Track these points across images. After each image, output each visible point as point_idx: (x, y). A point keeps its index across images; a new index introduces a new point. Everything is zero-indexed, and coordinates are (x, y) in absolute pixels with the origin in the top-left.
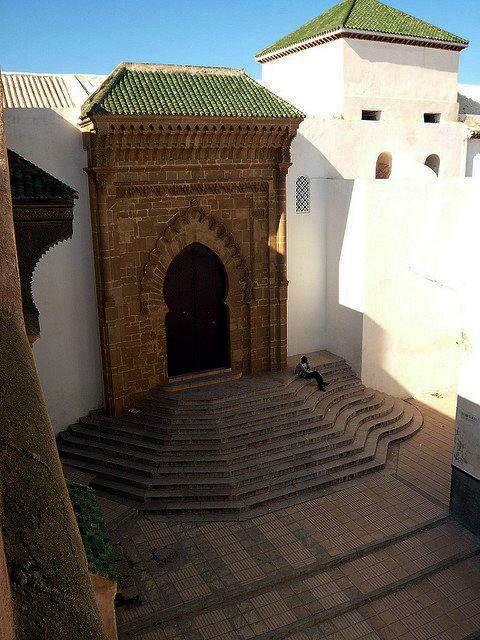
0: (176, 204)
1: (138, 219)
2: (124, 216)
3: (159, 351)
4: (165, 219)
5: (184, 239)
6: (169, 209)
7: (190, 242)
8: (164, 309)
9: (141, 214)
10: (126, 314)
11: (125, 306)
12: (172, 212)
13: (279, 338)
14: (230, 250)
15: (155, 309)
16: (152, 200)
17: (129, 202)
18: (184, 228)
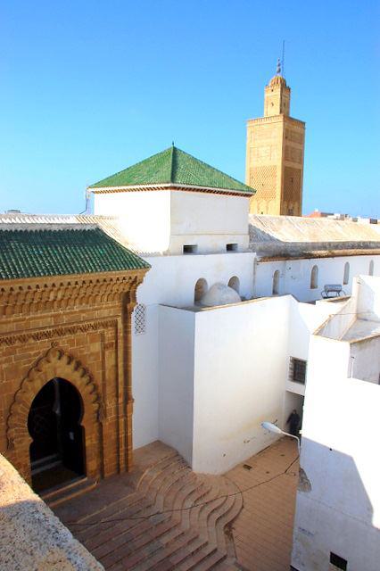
5: (46, 376)
6: (32, 353)
8: (28, 440)
12: (36, 355)
18: (45, 366)
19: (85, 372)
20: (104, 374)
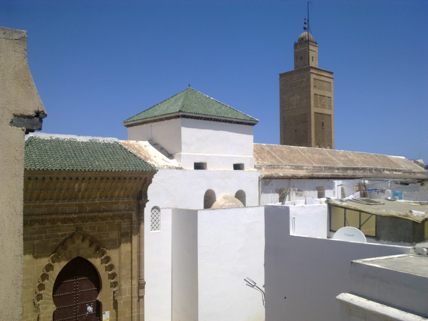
0: (67, 229)
1: (36, 242)
6: (60, 234)
7: (74, 256)
12: (63, 236)
16: (48, 228)
18: (70, 246)
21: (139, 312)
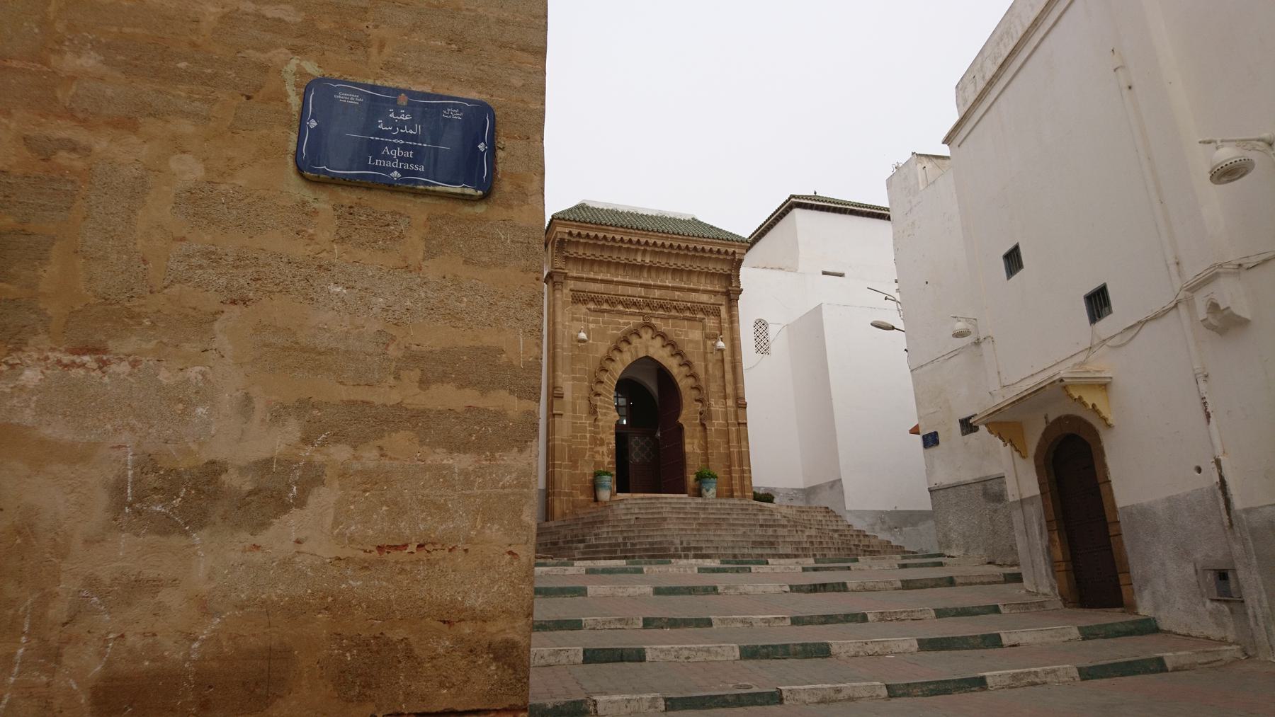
2: (578, 320)
3: (607, 460)
4: (618, 329)
9: (596, 322)
10: (574, 411)
11: (574, 404)
13: (741, 465)
14: (685, 370)
15: (605, 414)
17: (583, 308)
18: (635, 340)
19: (688, 364)
20: (706, 367)
21: (742, 479)
